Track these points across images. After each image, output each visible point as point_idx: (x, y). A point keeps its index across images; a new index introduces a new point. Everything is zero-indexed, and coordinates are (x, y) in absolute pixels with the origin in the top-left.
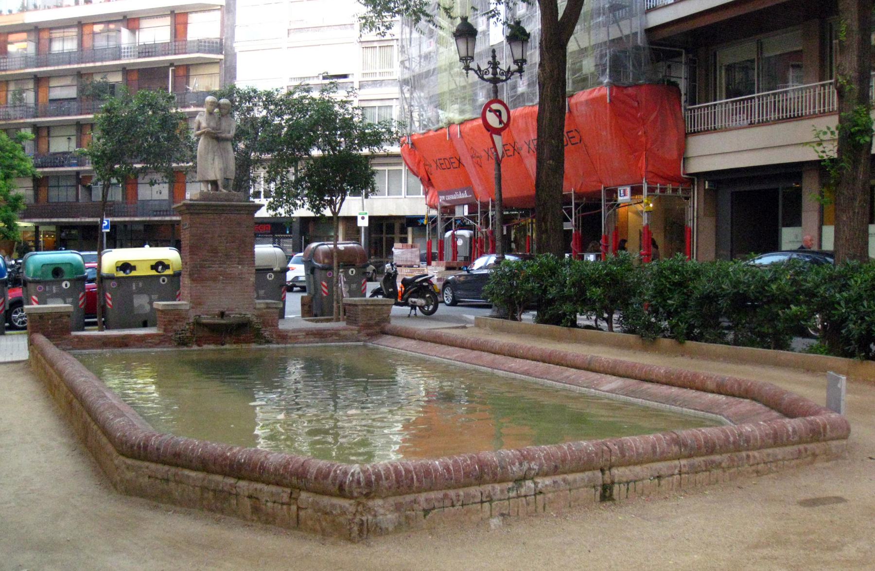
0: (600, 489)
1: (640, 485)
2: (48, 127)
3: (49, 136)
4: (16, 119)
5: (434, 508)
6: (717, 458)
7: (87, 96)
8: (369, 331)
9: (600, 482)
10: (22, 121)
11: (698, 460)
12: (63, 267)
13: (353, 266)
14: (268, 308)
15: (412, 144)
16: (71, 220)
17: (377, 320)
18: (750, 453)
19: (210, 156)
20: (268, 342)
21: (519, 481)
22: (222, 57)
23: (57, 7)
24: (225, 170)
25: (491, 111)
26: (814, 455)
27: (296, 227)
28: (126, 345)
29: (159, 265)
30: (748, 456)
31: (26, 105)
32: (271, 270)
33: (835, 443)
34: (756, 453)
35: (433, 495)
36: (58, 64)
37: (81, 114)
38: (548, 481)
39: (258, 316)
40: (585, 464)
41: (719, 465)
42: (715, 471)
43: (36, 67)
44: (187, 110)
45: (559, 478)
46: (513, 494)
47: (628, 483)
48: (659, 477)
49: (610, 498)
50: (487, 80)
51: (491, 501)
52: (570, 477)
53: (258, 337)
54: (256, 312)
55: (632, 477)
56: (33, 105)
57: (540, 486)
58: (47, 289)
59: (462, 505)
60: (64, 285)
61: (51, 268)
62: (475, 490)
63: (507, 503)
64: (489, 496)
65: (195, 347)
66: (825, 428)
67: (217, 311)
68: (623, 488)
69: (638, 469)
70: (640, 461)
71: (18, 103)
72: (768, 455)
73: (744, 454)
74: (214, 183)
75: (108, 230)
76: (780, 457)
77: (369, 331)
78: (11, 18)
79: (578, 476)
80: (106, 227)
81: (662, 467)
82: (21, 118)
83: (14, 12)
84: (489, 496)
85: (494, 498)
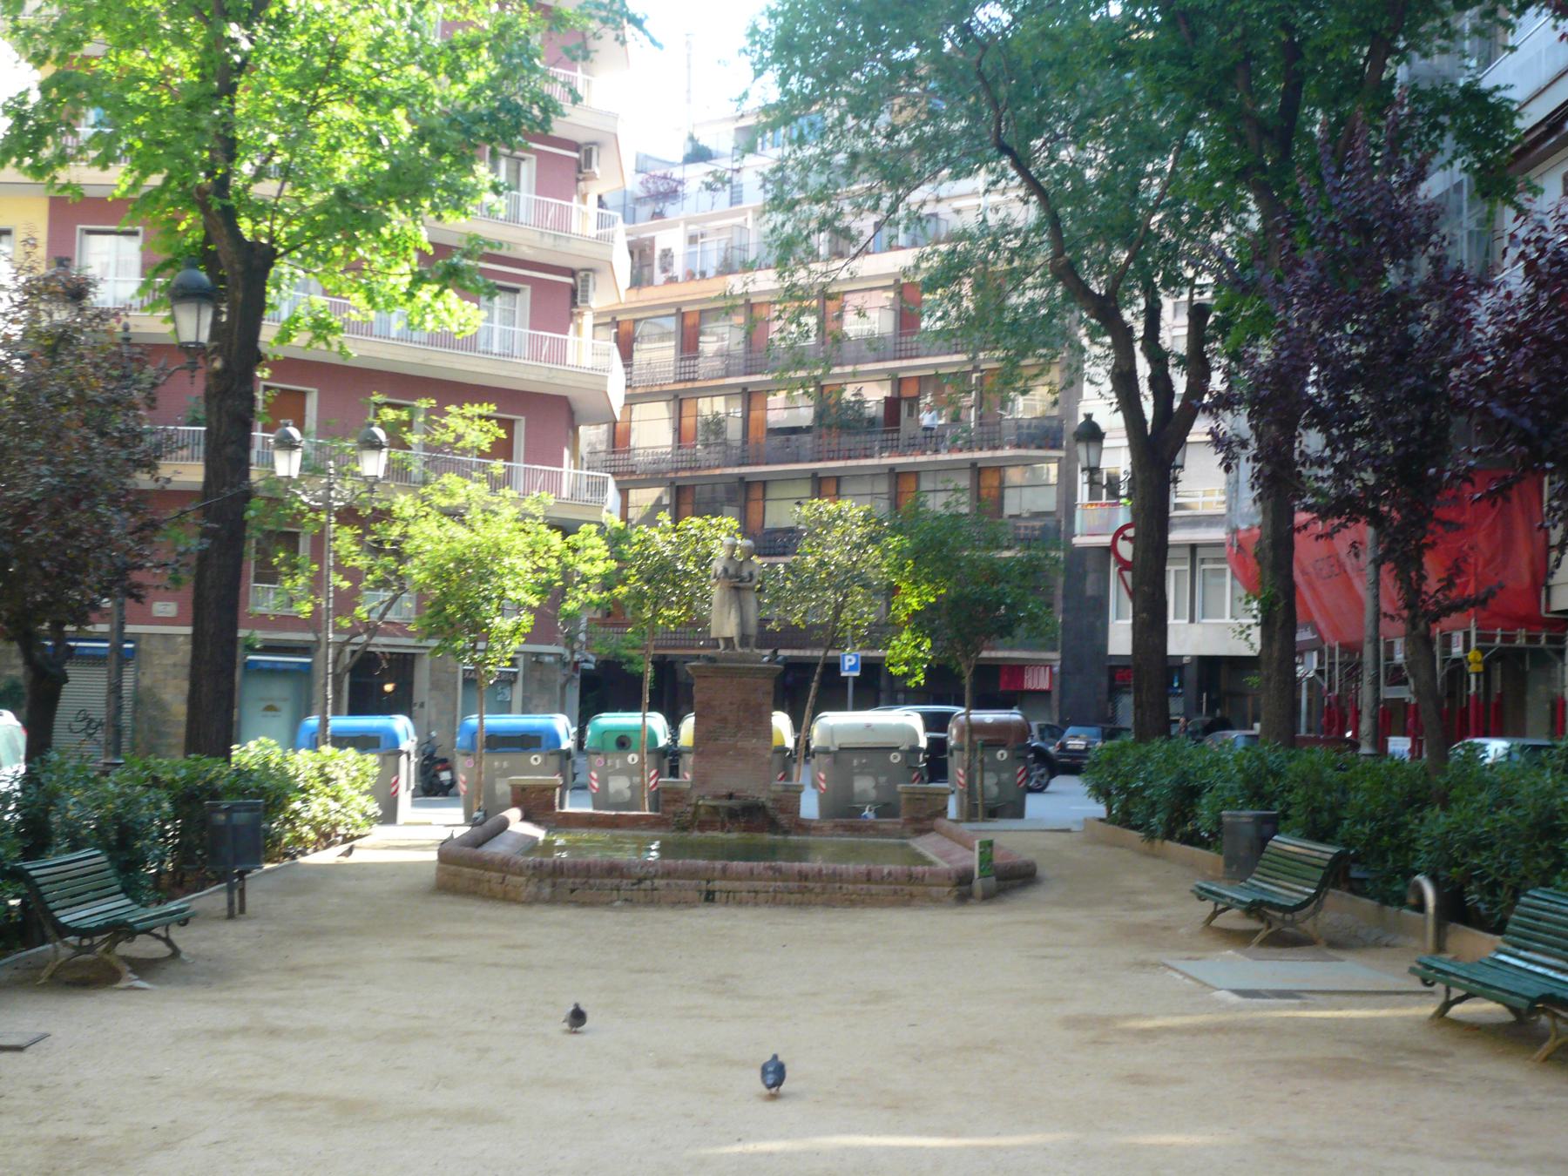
2: (764, 483)
3: (764, 499)
4: (709, 467)
6: (810, 885)
7: (829, 427)
8: (919, 826)
10: (718, 472)
11: (792, 885)
12: (630, 735)
15: (1239, 546)
16: (796, 653)
19: (726, 609)
20: (787, 832)
21: (640, 881)
24: (743, 623)
25: (1125, 538)
26: (911, 895)
27: (1191, 674)
31: (725, 443)
32: (896, 749)
33: (935, 889)
34: (851, 887)
35: (578, 881)
37: (820, 460)
38: (663, 882)
39: (774, 800)
40: (692, 874)
41: (811, 891)
43: (746, 374)
44: (999, 453)
45: (672, 882)
49: (713, 900)
52: (680, 882)
53: (773, 826)
54: (772, 796)
56: (739, 443)
58: (609, 763)
60: (630, 758)
61: (617, 735)
62: (607, 881)
67: (724, 792)
69: (737, 884)
71: (712, 438)
74: (728, 640)
75: (857, 674)
77: (919, 826)
78: (704, 285)
80: (852, 668)
81: (759, 885)
82: (718, 467)
83: (711, 273)
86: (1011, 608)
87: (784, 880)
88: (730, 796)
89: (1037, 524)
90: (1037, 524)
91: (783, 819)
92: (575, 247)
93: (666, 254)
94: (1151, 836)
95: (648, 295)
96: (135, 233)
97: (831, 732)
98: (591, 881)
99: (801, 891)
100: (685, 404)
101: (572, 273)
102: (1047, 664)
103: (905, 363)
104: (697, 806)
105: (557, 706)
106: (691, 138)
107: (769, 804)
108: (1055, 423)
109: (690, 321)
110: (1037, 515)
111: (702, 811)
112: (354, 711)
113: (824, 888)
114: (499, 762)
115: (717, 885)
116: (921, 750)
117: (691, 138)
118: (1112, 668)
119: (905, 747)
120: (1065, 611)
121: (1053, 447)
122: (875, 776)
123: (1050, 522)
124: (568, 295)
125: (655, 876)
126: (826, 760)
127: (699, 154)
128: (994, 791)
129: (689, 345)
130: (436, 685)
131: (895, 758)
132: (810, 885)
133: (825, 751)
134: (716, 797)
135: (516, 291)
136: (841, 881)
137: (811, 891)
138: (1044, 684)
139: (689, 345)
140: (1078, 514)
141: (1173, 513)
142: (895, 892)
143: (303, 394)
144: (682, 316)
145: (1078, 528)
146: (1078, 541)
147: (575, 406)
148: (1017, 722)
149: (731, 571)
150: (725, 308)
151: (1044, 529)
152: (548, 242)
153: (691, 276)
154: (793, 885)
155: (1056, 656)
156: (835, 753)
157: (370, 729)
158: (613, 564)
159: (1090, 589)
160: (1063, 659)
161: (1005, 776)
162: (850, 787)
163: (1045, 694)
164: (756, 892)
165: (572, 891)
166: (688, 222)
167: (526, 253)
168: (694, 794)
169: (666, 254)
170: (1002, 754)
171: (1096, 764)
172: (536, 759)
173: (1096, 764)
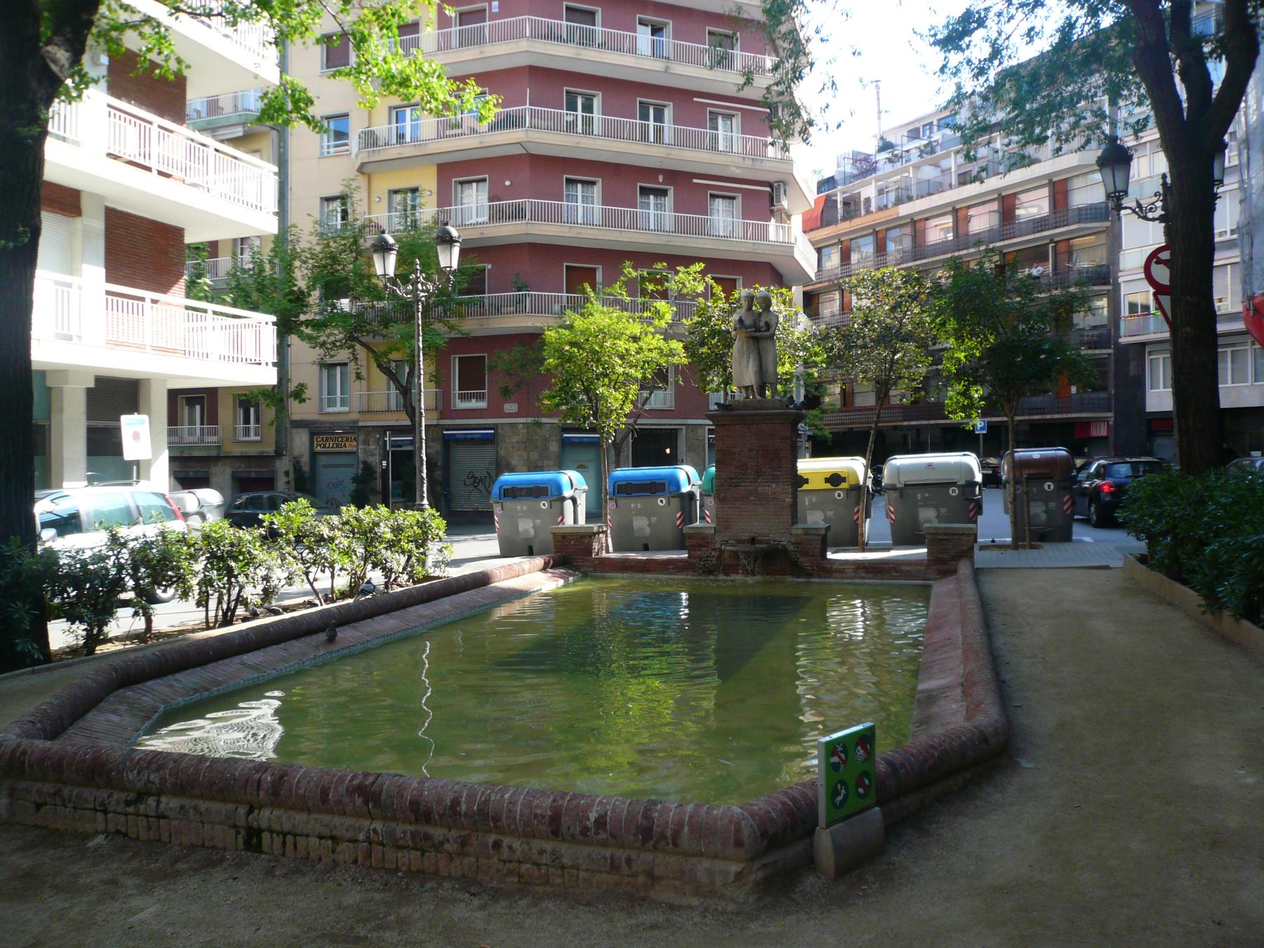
0: (243, 832)
1: (301, 842)
5: (45, 804)
6: (438, 833)
9: (241, 821)
13: (1050, 478)
14: (806, 534)
17: (952, 552)
18: (506, 841)
20: (809, 575)
21: (141, 796)
22: (1108, 224)
23: (930, 194)
25: (1159, 262)
28: (648, 571)
29: (835, 479)
30: (497, 845)
32: (954, 484)
34: (516, 844)
36: (935, 255)
41: (438, 847)
42: (431, 854)
45: (187, 802)
46: (131, 809)
47: (285, 835)
48: (333, 838)
50: (1153, 220)
51: (105, 812)
52: (203, 805)
53: (796, 569)
55: (287, 827)
57: (162, 806)
59: (75, 808)
62: (88, 793)
63: (123, 818)
64: (102, 804)
65: (721, 577)
66: (677, 833)
67: (746, 536)
68: (278, 840)
69: (300, 817)
70: (303, 806)
72: (541, 852)
73: (492, 838)
76: (566, 861)
79: (215, 806)
80: (982, 429)
84: (102, 804)
85: (111, 808)
86: (1050, 353)
87: (385, 819)
88: (753, 540)
89: (1095, 333)
90: (1095, 333)
91: (804, 561)
92: (766, 165)
93: (868, 200)
94: (1214, 603)
95: (857, 223)
96: (484, 180)
97: (898, 471)
98: (66, 791)
99: (422, 844)
100: (824, 251)
101: (770, 185)
102: (1105, 420)
103: (1007, 242)
104: (721, 550)
105: (177, 454)
106: (882, 138)
107: (791, 548)
108: (1104, 269)
109: (880, 236)
110: (1095, 328)
111: (726, 555)
112: (636, 464)
113: (464, 842)
114: (635, 504)
115: (265, 817)
116: (977, 483)
117: (882, 138)
118: (1148, 420)
119: (962, 482)
120: (1116, 386)
121: (1104, 284)
122: (936, 507)
123: (1104, 331)
124: (767, 202)
125: (159, 793)
126: (894, 495)
127: (885, 146)
128: (1044, 517)
129: (881, 248)
130: (690, 449)
131: (954, 492)
132: (438, 833)
133: (893, 488)
134: (739, 542)
135: (733, 198)
136: (498, 829)
137: (438, 847)
138: (1104, 433)
139: (881, 248)
140: (1122, 324)
141: (1217, 239)
142: (614, 866)
143: (594, 270)
144: (876, 233)
145: (1122, 332)
146: (1123, 340)
147: (781, 270)
148: (1062, 457)
149: (748, 322)
150: (899, 223)
151: (1100, 336)
152: (748, 163)
153: (880, 209)
154: (403, 829)
155: (1111, 414)
156: (901, 489)
157: (659, 477)
158: (568, 311)
159: (1133, 370)
160: (1115, 417)
161: (1052, 505)
162: (916, 515)
163: (1105, 438)
164: (334, 838)
165: (38, 806)
166: (877, 180)
167: (737, 173)
168: (718, 538)
169: (868, 200)
170: (1049, 486)
171: (1136, 500)
172: (661, 501)
173: (1136, 500)
